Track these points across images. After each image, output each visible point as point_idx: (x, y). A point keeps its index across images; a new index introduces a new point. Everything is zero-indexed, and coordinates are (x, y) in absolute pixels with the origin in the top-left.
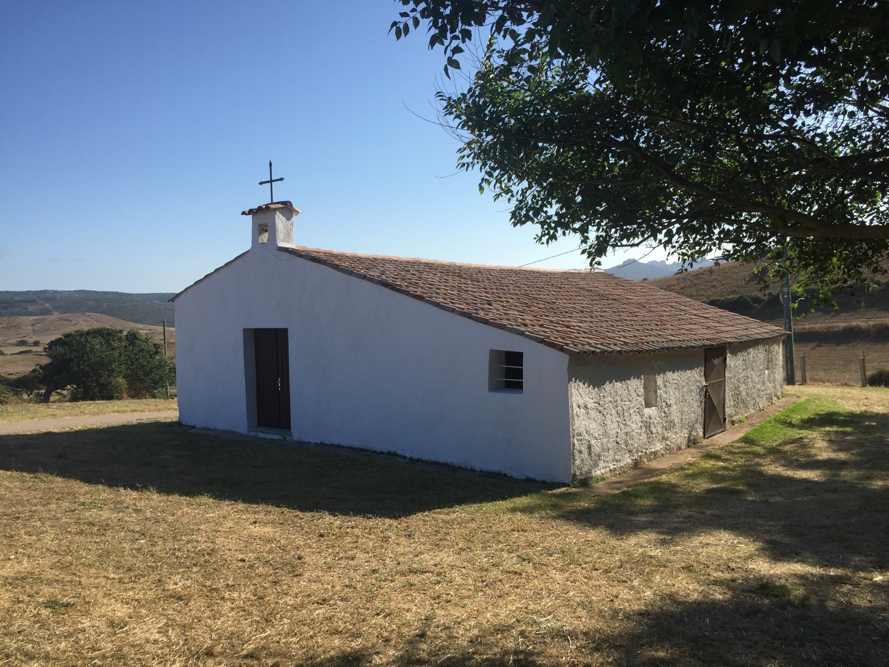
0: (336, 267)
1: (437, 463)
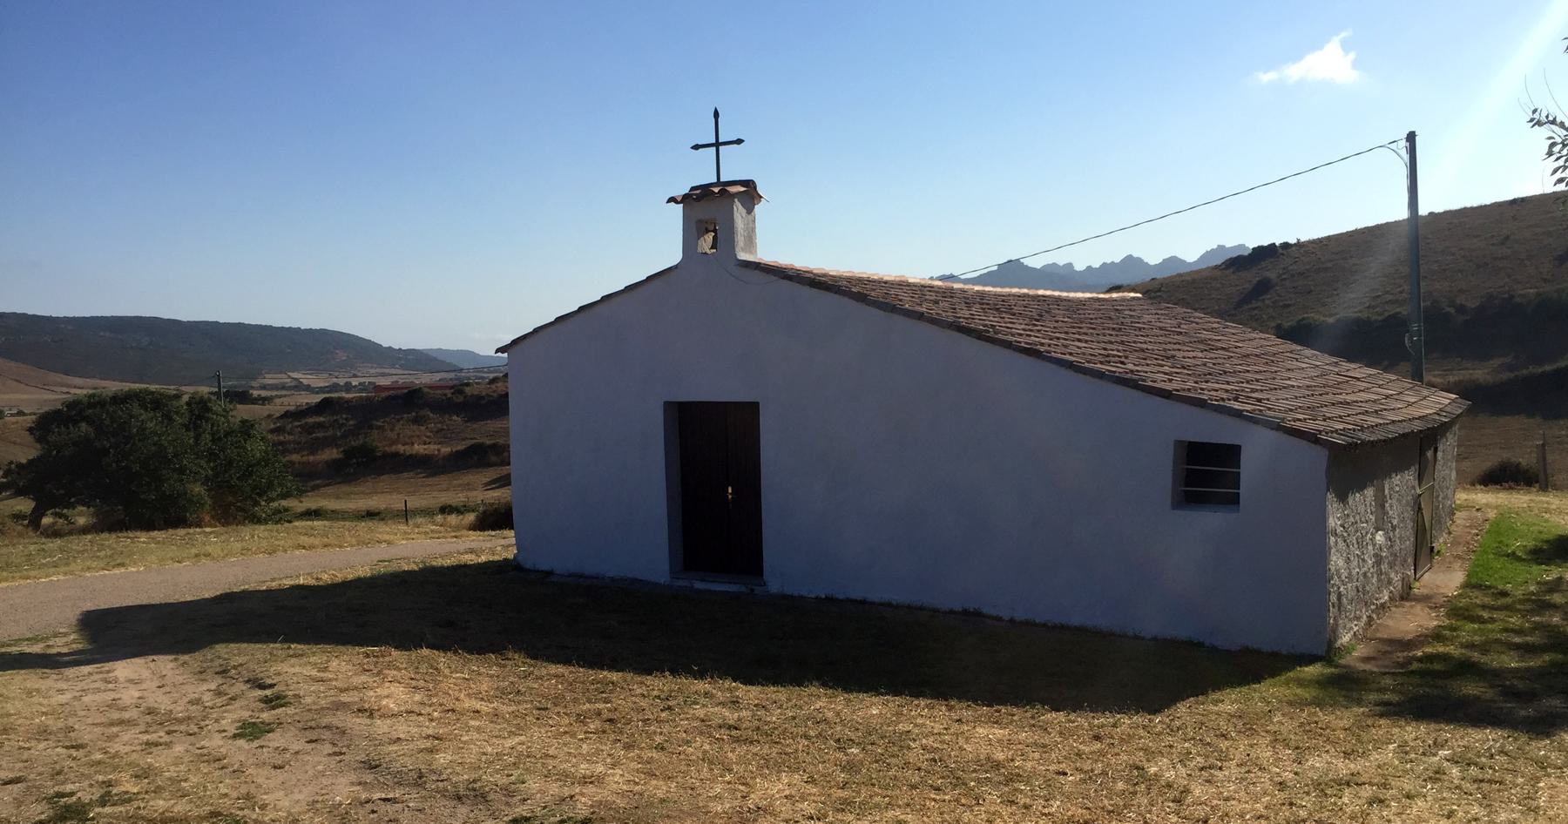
0: (861, 298)
1: (1063, 628)
